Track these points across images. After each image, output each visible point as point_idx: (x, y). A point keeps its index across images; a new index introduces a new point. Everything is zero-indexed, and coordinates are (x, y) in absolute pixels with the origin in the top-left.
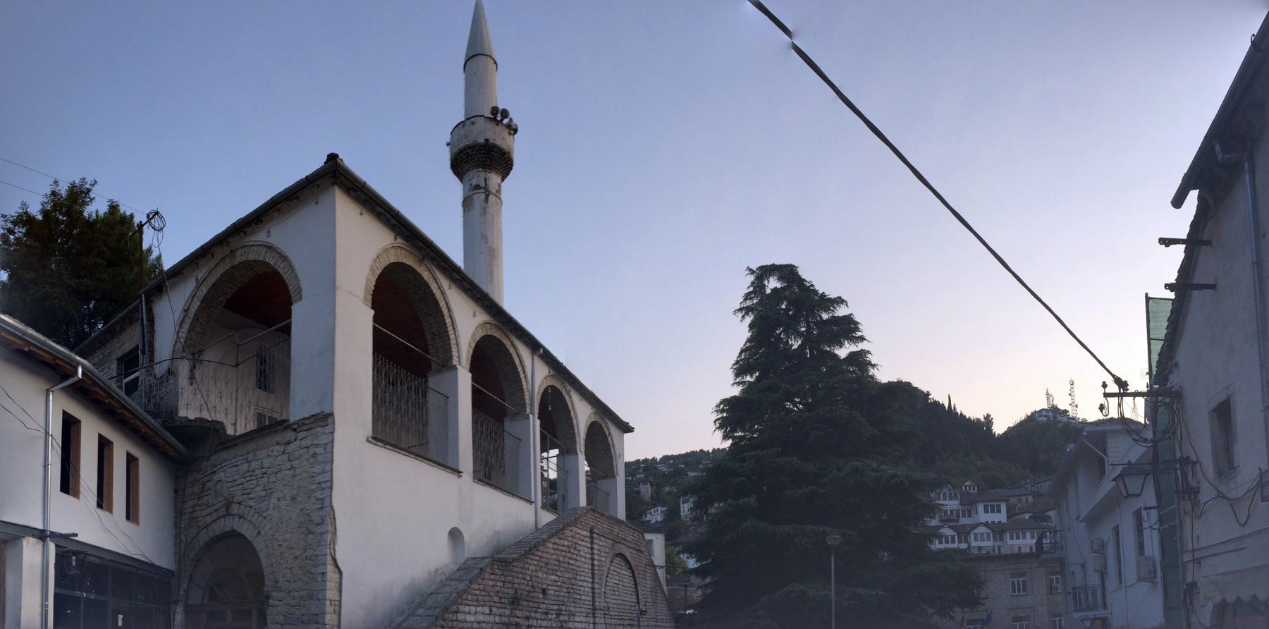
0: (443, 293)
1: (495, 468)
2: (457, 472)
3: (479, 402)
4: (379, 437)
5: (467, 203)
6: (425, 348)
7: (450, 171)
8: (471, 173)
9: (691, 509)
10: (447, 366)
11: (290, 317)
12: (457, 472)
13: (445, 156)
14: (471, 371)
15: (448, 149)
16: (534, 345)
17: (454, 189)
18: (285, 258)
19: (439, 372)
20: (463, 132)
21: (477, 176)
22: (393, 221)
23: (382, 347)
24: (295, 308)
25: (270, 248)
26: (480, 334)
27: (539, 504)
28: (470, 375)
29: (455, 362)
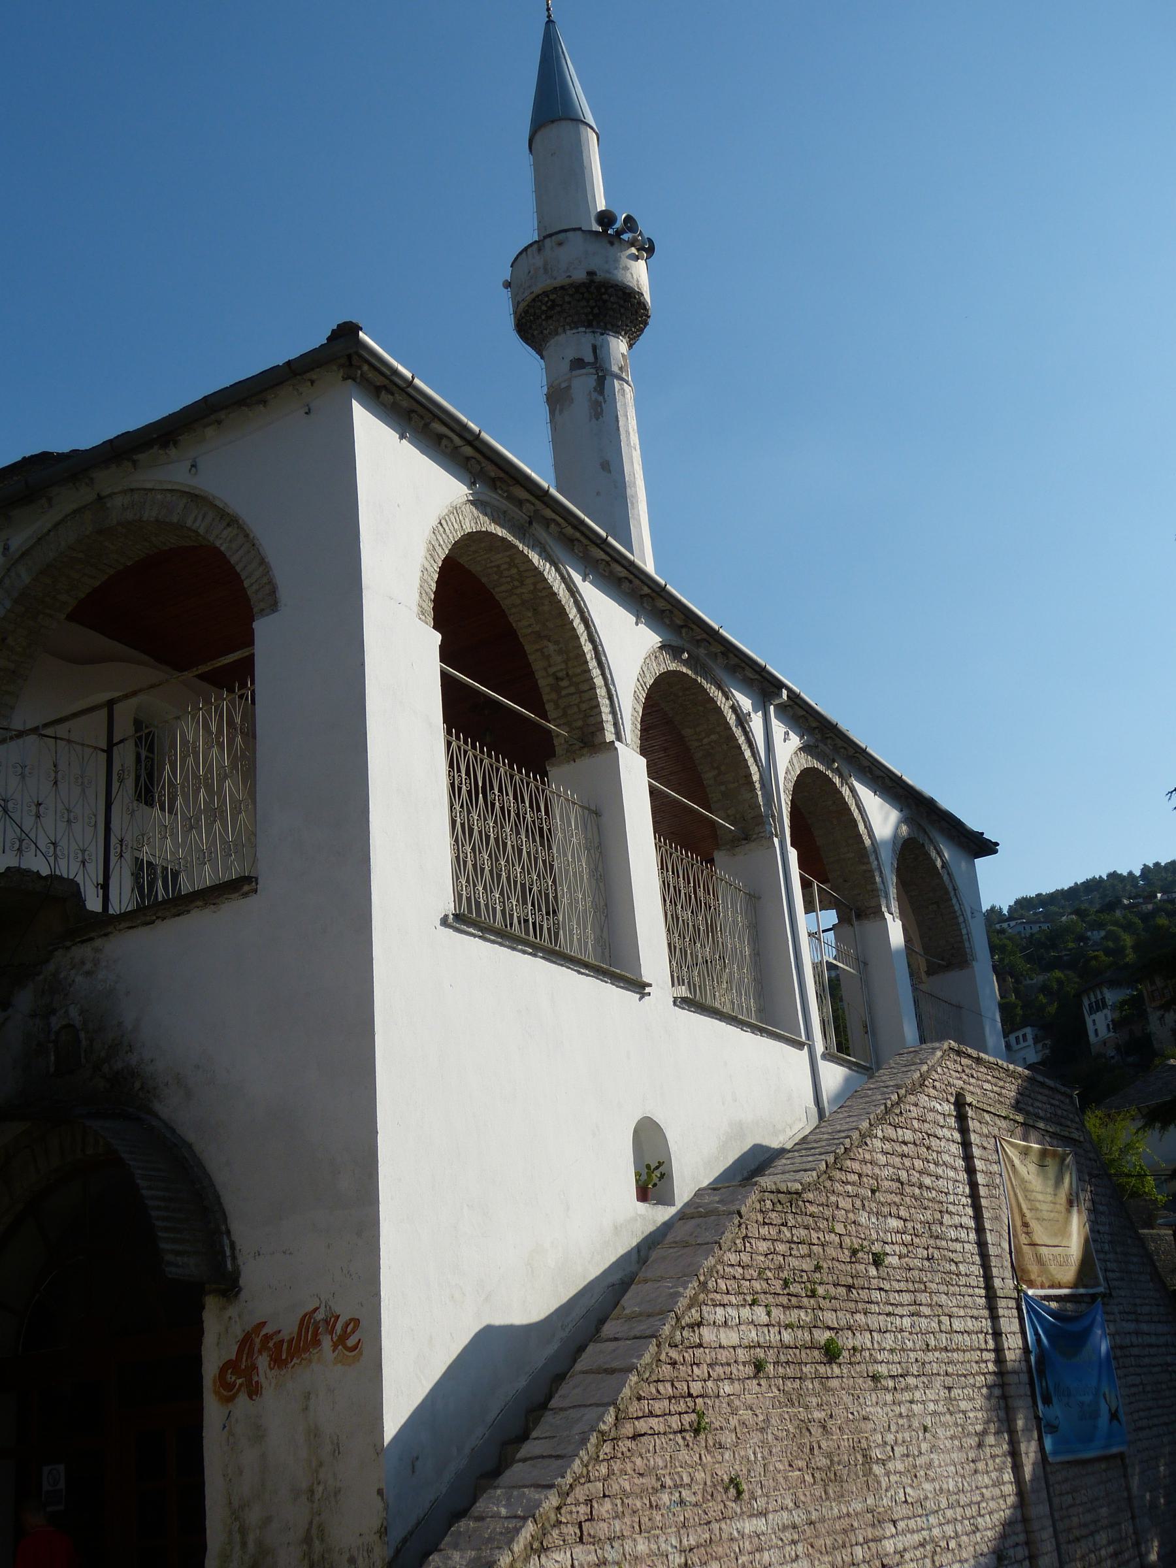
0: (573, 591)
1: (731, 982)
2: (639, 987)
3: (670, 824)
4: (464, 919)
5: (557, 398)
6: (534, 701)
7: (515, 336)
8: (561, 338)
9: (1116, 1025)
10: (590, 740)
11: (251, 643)
12: (639, 987)
13: (502, 312)
14: (643, 752)
15: (506, 295)
16: (765, 686)
17: (528, 371)
18: (232, 521)
19: (572, 755)
20: (538, 261)
21: (572, 343)
22: (468, 451)
23: (462, 713)
24: (262, 627)
25: (197, 499)
26: (657, 669)
27: (820, 1048)
28: (643, 761)
29: (610, 736)
